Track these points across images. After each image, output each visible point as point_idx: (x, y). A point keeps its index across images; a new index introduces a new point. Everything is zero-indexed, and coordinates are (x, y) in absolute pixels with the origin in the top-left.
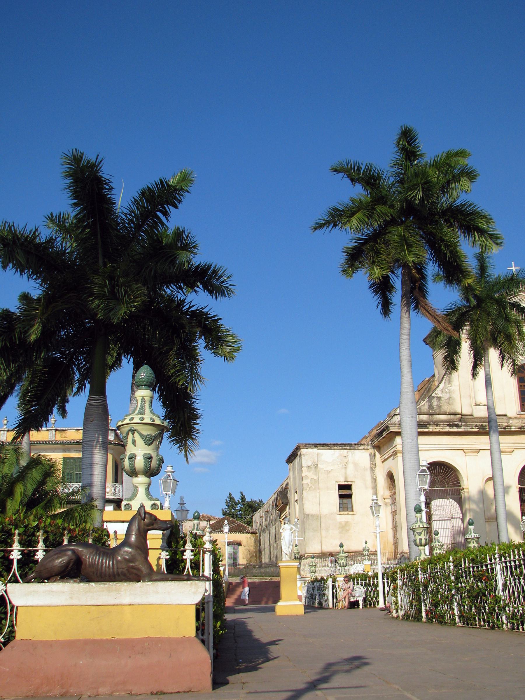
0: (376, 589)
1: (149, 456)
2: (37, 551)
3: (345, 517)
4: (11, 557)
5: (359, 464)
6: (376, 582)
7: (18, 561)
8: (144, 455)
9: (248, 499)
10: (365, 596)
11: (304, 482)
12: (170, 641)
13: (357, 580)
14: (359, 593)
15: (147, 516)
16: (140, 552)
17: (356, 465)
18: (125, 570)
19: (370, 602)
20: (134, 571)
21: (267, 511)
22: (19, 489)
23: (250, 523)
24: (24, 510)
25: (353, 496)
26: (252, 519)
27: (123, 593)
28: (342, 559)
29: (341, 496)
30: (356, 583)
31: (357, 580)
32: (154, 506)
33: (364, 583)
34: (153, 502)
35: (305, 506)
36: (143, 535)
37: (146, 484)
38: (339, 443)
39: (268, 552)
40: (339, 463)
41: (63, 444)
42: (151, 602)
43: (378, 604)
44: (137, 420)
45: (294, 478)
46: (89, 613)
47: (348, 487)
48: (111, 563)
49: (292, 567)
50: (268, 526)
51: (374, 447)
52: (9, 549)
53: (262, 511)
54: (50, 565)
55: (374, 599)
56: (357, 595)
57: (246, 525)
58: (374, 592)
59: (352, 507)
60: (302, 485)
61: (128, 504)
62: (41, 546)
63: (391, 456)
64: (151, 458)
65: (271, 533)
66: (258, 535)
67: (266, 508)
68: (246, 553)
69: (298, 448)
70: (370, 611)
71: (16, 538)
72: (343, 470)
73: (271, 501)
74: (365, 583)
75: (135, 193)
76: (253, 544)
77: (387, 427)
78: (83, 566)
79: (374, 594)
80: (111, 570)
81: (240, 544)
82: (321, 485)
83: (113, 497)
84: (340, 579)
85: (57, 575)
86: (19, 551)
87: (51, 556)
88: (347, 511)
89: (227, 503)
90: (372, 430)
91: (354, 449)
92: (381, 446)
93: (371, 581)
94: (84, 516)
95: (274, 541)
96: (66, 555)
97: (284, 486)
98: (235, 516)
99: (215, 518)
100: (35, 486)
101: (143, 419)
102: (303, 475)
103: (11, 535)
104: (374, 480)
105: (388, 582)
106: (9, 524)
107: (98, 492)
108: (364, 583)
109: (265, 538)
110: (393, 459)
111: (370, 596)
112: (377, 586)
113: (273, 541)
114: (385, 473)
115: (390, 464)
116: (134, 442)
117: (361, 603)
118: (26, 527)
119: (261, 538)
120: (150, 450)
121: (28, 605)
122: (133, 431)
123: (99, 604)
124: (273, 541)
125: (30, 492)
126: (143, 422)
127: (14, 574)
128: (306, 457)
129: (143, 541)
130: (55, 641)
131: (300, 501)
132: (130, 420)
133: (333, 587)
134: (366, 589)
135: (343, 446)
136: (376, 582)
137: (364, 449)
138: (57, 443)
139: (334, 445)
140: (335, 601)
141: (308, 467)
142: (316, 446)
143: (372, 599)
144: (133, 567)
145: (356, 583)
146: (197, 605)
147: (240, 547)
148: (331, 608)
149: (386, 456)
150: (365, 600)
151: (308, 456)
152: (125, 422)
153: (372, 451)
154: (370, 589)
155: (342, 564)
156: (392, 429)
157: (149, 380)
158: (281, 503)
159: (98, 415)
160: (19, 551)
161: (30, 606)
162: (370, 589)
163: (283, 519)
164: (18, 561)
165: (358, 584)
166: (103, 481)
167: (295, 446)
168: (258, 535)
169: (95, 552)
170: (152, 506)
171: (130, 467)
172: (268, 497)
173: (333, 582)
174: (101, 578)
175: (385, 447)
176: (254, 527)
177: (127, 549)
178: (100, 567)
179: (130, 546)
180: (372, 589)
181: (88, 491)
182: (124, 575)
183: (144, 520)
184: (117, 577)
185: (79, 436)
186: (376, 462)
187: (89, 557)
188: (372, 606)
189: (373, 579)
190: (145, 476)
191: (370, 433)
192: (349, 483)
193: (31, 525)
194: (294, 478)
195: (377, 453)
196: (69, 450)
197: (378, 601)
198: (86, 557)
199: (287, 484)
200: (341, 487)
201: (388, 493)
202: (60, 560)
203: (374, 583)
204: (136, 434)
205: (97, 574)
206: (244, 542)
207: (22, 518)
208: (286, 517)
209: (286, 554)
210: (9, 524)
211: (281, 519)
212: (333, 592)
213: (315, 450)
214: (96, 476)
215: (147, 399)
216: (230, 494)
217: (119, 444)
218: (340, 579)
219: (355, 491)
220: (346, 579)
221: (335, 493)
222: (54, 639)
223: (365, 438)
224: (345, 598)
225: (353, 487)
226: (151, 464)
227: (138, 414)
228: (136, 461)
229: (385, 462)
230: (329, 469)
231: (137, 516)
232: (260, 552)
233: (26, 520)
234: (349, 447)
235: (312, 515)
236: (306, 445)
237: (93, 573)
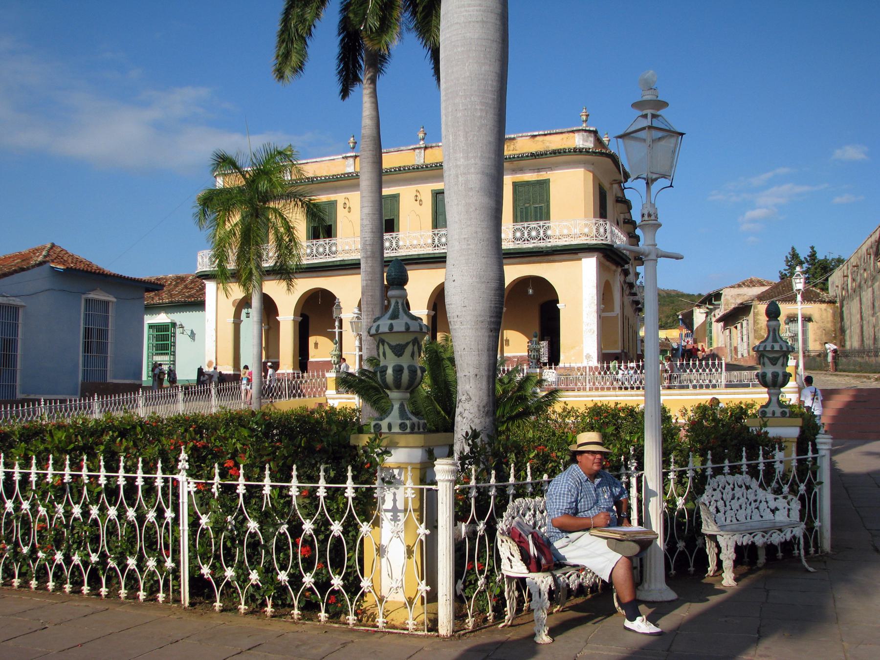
9: (820, 256)
21: (857, 266)
23: (825, 289)
39: (858, 331)
50: (858, 290)
53: (845, 267)
57: (818, 291)
65: (864, 300)
66: (838, 305)
68: (819, 332)
76: (830, 318)
83: (595, 242)
89: (787, 261)
95: (871, 312)
99: (769, 283)
113: (867, 312)
119: (844, 309)
124: (867, 312)
168: (838, 305)
196: (521, 170)
206: (816, 316)
216: (793, 248)
217: (601, 154)
232: (842, 331)
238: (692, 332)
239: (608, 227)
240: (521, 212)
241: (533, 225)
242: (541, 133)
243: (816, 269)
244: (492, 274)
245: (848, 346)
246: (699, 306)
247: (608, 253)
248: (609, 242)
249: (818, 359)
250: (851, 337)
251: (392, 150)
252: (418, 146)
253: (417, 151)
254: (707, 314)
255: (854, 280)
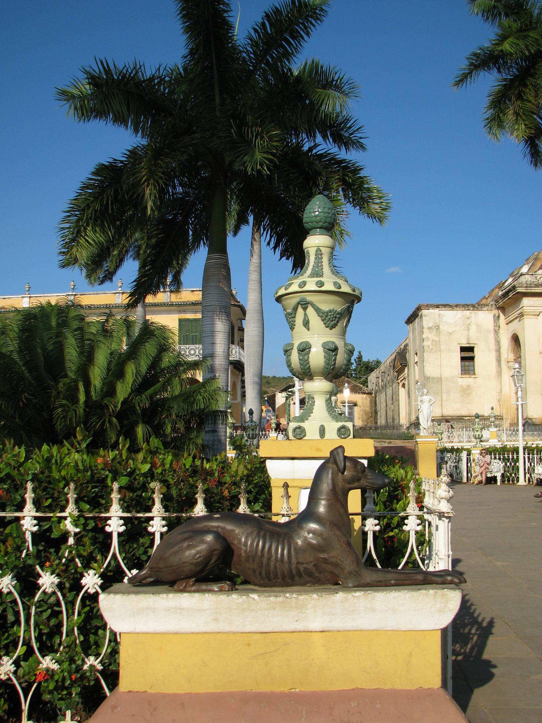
0: (515, 464)
1: (333, 347)
2: (152, 518)
3: (467, 380)
4: (108, 529)
5: (480, 325)
6: (515, 457)
7: (120, 535)
8: (324, 345)
9: (365, 359)
10: (503, 472)
11: (425, 343)
12: (395, 695)
13: (495, 455)
14: (497, 468)
15: (348, 464)
16: (338, 533)
17: (478, 326)
18: (310, 566)
19: (509, 477)
20: (329, 567)
21: (384, 372)
22: (130, 370)
23: (365, 383)
24: (127, 446)
25: (476, 359)
26: (367, 379)
27: (309, 611)
28: (477, 431)
29: (463, 359)
30: (493, 457)
31: (495, 455)
32: (343, 430)
33: (502, 457)
34: (340, 424)
35: (426, 369)
36: (339, 499)
37: (326, 393)
38: (462, 303)
39: (384, 413)
40: (461, 325)
41: (179, 305)
42: (362, 627)
43: (518, 481)
44: (311, 286)
45: (414, 340)
46: (249, 645)
47: (471, 349)
48: (286, 552)
49: (430, 443)
50: (384, 387)
51: (498, 308)
52: (103, 515)
53: (378, 371)
54: (175, 560)
55: (513, 475)
56: (495, 470)
57: (361, 386)
58: (513, 467)
59: (474, 370)
60: (423, 347)
61: (299, 427)
62: (157, 510)
63: (517, 318)
64: (335, 350)
65: (388, 394)
66: (373, 395)
67: (382, 368)
68: (361, 413)
69: (419, 309)
70: (508, 487)
71: (115, 496)
72: (466, 332)
73: (388, 362)
74: (504, 457)
75: (258, 17)
76: (368, 404)
77: (514, 287)
78: (235, 558)
79: (513, 469)
80: (287, 566)
81: (355, 405)
82: (443, 347)
84: (476, 453)
85: (188, 577)
86: (121, 518)
87: (177, 544)
88: (469, 374)
90: (493, 290)
91: (478, 310)
92: (506, 307)
93: (510, 455)
94: (209, 399)
95: (391, 402)
96: (203, 542)
97: (402, 347)
98: (349, 376)
100: (149, 363)
101: (321, 284)
102: (424, 336)
103: (107, 491)
104: (498, 343)
105: (529, 458)
106: (103, 469)
107: (221, 363)
108: (502, 457)
109: (381, 399)
110: (519, 321)
111: (508, 472)
112: (517, 460)
113: (389, 402)
114: (510, 336)
115: (515, 326)
116: (306, 324)
117: (499, 479)
118: (130, 474)
119: (377, 398)
120: (331, 336)
121: (137, 630)
122: (305, 304)
123: (265, 630)
124: (389, 402)
125: (144, 369)
126: (323, 289)
127: (114, 555)
128: (428, 318)
129: (342, 510)
130: (190, 696)
131: (421, 363)
132: (300, 286)
133: (468, 460)
134: (504, 464)
135: (466, 306)
136: (515, 457)
137: (488, 310)
138: (172, 305)
139: (457, 306)
140: (469, 475)
141: (430, 328)
142: (437, 306)
143: (511, 475)
144: (325, 560)
145: (493, 457)
146: (444, 631)
147: (356, 408)
148: (465, 483)
149: (511, 318)
150: (503, 475)
151: (429, 316)
152: (291, 290)
153: (496, 312)
154: (508, 464)
155: (477, 436)
156: (519, 290)
157: (328, 220)
158: (399, 364)
159: (219, 273)
160: (121, 518)
161: (143, 633)
162: (508, 464)
163: (401, 381)
164: (120, 535)
165: (495, 458)
166: (226, 351)
167: (416, 306)
168: (373, 395)
169: (256, 532)
170: (339, 430)
171: (301, 364)
172: (386, 357)
173: (467, 455)
174: (269, 580)
175: (511, 309)
176: (370, 387)
177: (313, 526)
178: (265, 561)
179: (318, 519)
180: (511, 464)
181: (209, 363)
182: (310, 574)
183: (343, 473)
184: (297, 578)
185: (198, 296)
186: (501, 324)
187: (244, 539)
188: (511, 482)
189: (513, 454)
190: (326, 378)
191: (490, 293)
192: (472, 345)
193: (140, 470)
194: (414, 340)
195: (501, 315)
196: (184, 312)
197: (518, 478)
198: (240, 540)
199: (406, 346)
200: (463, 349)
201: (512, 357)
202: (193, 551)
203: (513, 458)
204: (310, 310)
205: (260, 573)
206: (359, 403)
207: (124, 458)
208: (404, 378)
209: (425, 428)
210: (103, 469)
211: (399, 381)
212: (467, 466)
213: (436, 311)
214: (219, 345)
215: (325, 251)
218: (476, 453)
219: (477, 353)
220: (483, 451)
221: (458, 355)
222: (187, 692)
223: (485, 298)
224: (481, 474)
225: (475, 349)
226: (335, 360)
227: (312, 275)
228: (311, 356)
229: (510, 324)
230: (450, 330)
231: (330, 465)
232: (376, 412)
233: (131, 462)
234: (472, 308)
235: (433, 378)
236: (427, 306)
237: (254, 571)
238: (274, 409)
239: (237, 350)
240: (184, 337)
241: (192, 346)
242: (198, 289)
243: (361, 368)
244: (259, 408)
245: (379, 424)
246: (282, 391)
247: (237, 365)
248: (237, 359)
249: (360, 431)
250: (380, 417)
251: (100, 292)
252: (118, 292)
253: (118, 294)
254: (287, 398)
255: (382, 381)
